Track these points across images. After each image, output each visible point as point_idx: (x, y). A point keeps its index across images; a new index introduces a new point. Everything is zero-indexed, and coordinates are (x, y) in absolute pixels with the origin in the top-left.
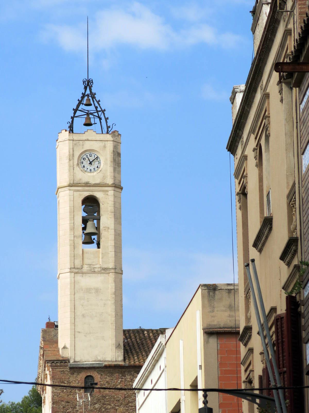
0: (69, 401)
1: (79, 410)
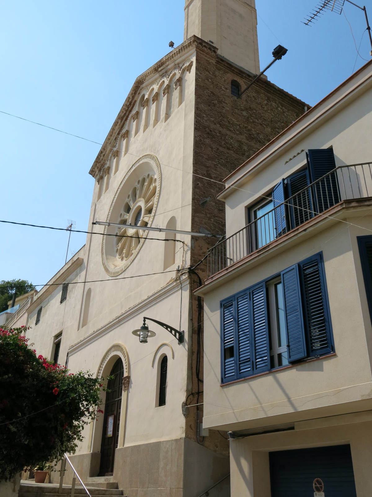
1: (226, 108)
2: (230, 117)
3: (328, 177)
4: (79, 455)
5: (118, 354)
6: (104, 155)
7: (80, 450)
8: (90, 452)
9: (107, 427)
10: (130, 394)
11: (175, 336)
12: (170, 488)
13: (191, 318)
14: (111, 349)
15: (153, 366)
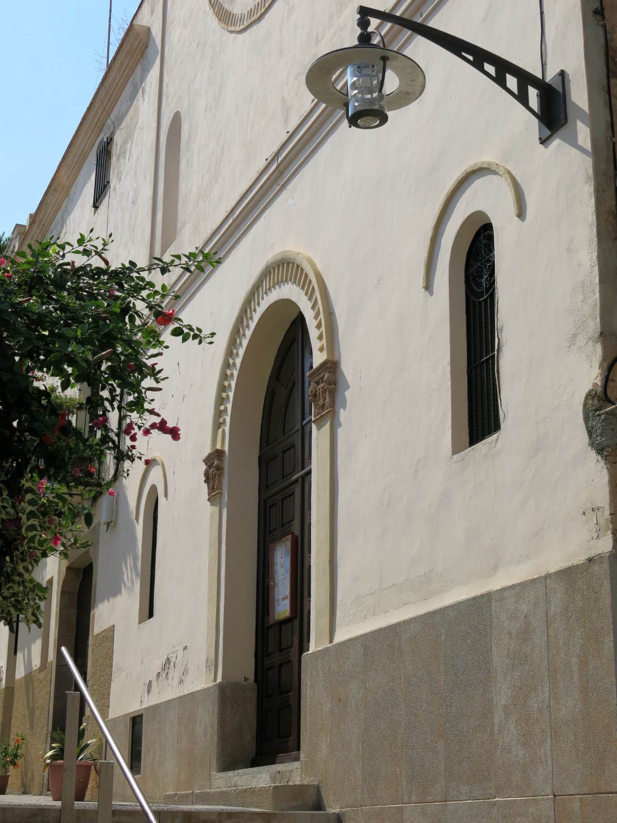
4: (180, 698)
5: (285, 297)
7: (181, 682)
8: (215, 680)
10: (341, 433)
11: (522, 98)
12: (555, 796)
13: (597, 5)
14: (258, 289)
15: (428, 286)
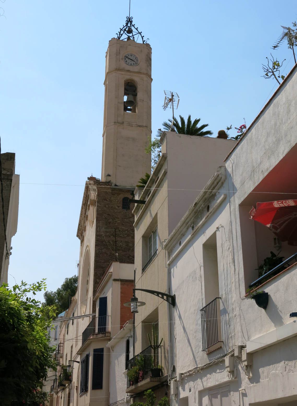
0: (110, 214)
1: (118, 221)
2: (120, 227)
3: (102, 328)
6: (81, 226)
9: (88, 384)
